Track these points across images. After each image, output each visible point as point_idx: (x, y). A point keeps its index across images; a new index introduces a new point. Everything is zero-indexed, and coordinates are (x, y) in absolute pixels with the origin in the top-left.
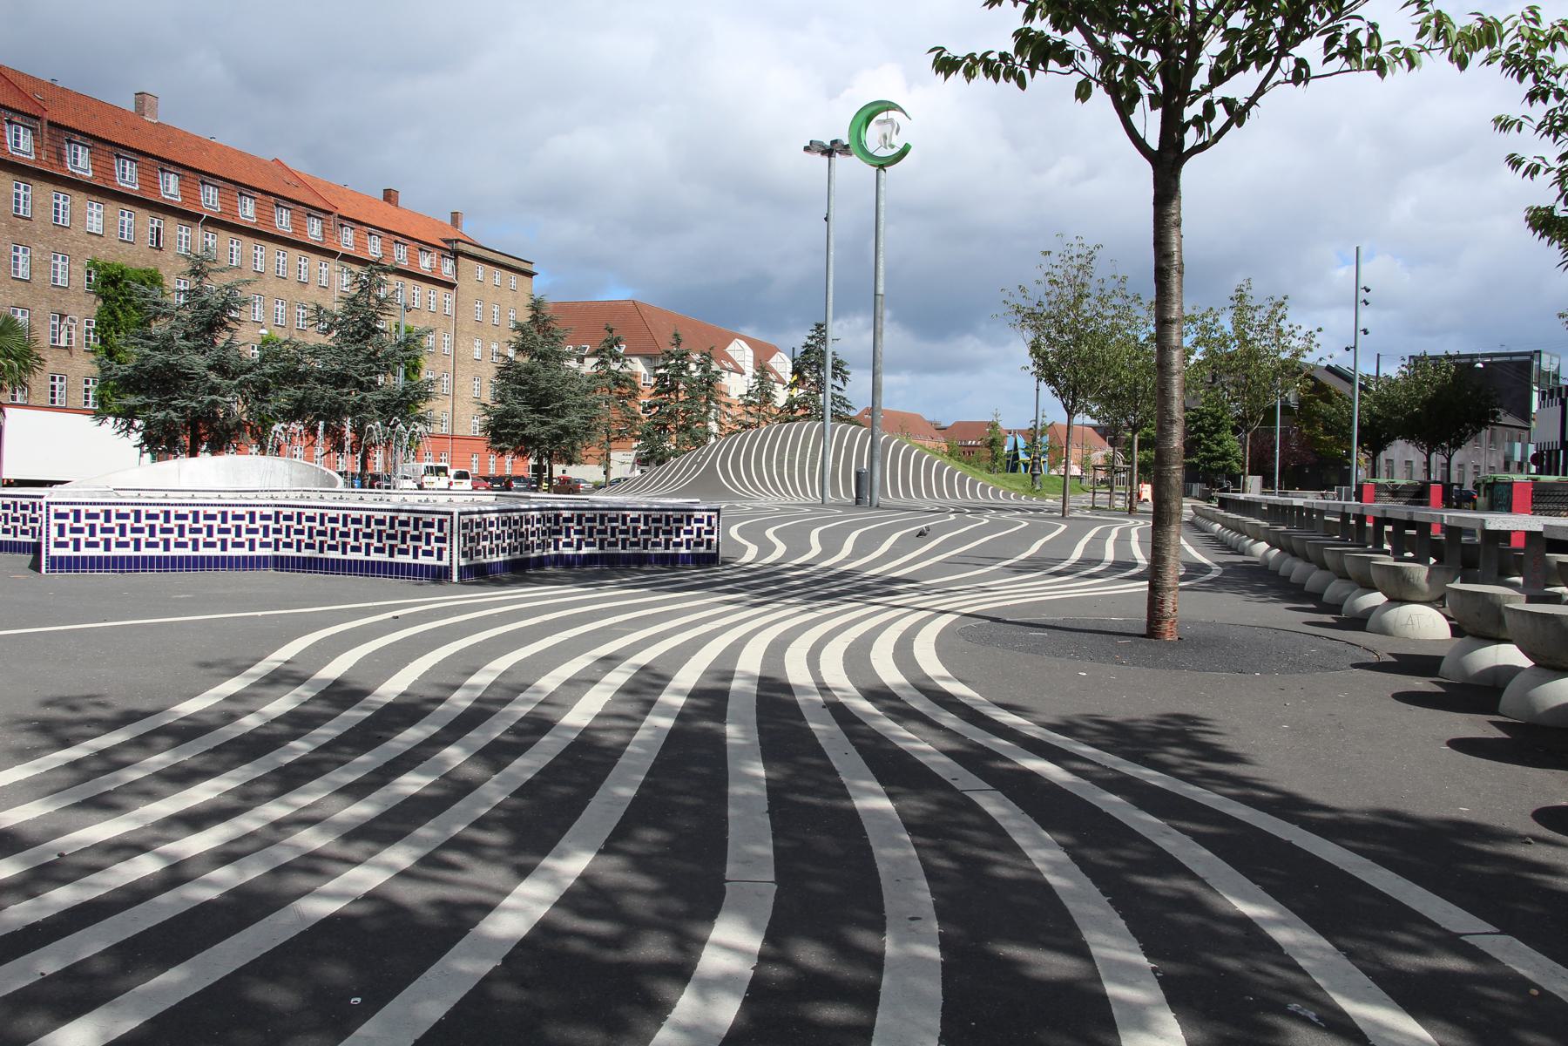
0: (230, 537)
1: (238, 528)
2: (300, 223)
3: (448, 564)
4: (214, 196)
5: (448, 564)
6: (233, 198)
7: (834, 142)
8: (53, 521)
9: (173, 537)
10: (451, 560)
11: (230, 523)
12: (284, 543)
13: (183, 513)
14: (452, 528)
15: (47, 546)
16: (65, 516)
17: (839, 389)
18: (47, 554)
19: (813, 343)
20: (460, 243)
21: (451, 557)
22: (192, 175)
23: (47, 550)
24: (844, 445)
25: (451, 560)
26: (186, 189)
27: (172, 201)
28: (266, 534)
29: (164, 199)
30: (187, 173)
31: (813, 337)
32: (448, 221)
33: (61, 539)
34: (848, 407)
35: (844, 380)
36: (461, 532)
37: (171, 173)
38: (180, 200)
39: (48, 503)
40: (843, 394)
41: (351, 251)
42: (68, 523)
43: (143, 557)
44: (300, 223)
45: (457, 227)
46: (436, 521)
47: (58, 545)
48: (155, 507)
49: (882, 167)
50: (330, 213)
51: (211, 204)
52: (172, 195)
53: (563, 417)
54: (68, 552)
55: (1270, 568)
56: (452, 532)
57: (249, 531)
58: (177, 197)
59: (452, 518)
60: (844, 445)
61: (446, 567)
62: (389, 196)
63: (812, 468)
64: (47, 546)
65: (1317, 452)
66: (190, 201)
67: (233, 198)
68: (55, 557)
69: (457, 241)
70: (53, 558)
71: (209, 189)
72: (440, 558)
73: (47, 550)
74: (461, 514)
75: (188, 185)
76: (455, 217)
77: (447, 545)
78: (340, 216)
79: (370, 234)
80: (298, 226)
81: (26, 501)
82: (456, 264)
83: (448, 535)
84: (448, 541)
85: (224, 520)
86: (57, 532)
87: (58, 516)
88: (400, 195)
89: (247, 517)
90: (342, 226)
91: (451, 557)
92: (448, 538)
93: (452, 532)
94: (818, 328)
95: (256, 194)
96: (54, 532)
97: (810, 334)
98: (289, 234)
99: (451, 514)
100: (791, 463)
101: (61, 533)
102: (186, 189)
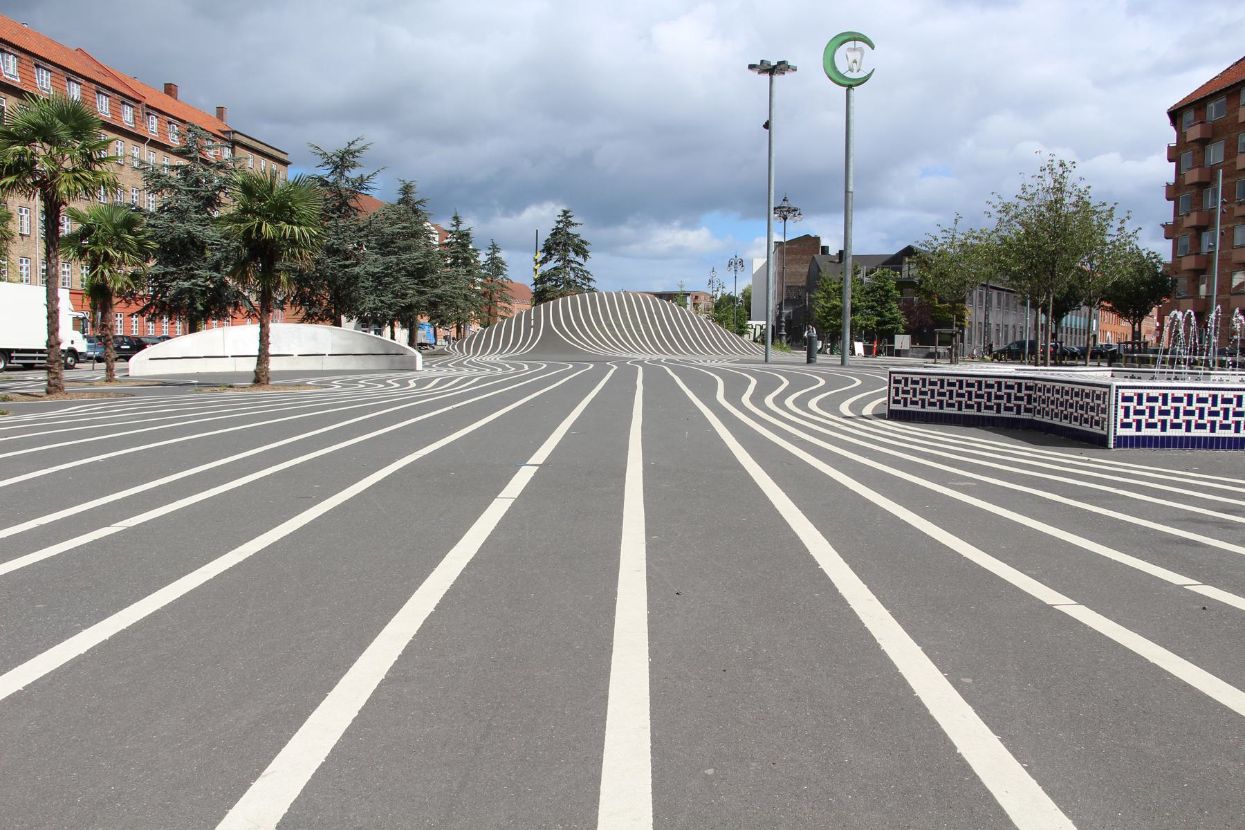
1: (1226, 411)
2: (117, 110)
4: (47, 80)
6: (63, 83)
7: (780, 63)
8: (1120, 404)
15: (1115, 427)
17: (580, 265)
18: (1115, 434)
19: (561, 225)
20: (236, 134)
22: (27, 57)
23: (1115, 430)
24: (654, 311)
26: (23, 71)
27: (13, 81)
29: (5, 78)
30: (23, 56)
31: (561, 221)
32: (214, 114)
33: (1126, 420)
34: (589, 279)
35: (585, 257)
37: (11, 54)
38: (19, 81)
39: (1117, 387)
40: (584, 268)
41: (156, 137)
43: (1192, 437)
44: (117, 110)
45: (222, 120)
47: (1125, 425)
48: (1130, 390)
49: (850, 87)
50: (138, 102)
51: (45, 87)
52: (12, 76)
54: (1131, 432)
58: (15, 77)
60: (654, 311)
62: (170, 89)
63: (638, 331)
64: (1115, 427)
65: (933, 317)
66: (29, 83)
67: (63, 83)
68: (1121, 436)
69: (234, 132)
70: (892, 410)
71: (42, 73)
73: (1115, 430)
75: (25, 67)
76: (220, 112)
77: (1106, 416)
78: (148, 106)
79: (170, 123)
80: (116, 112)
81: (916, 378)
82: (233, 152)
84: (1107, 413)
86: (1123, 414)
87: (1125, 399)
89: (1185, 399)
90: (148, 114)
94: (565, 214)
95: (80, 80)
96: (1121, 413)
97: (559, 219)
98: (108, 119)
99: (1109, 387)
100: (619, 326)
101: (1127, 415)
102: (23, 71)
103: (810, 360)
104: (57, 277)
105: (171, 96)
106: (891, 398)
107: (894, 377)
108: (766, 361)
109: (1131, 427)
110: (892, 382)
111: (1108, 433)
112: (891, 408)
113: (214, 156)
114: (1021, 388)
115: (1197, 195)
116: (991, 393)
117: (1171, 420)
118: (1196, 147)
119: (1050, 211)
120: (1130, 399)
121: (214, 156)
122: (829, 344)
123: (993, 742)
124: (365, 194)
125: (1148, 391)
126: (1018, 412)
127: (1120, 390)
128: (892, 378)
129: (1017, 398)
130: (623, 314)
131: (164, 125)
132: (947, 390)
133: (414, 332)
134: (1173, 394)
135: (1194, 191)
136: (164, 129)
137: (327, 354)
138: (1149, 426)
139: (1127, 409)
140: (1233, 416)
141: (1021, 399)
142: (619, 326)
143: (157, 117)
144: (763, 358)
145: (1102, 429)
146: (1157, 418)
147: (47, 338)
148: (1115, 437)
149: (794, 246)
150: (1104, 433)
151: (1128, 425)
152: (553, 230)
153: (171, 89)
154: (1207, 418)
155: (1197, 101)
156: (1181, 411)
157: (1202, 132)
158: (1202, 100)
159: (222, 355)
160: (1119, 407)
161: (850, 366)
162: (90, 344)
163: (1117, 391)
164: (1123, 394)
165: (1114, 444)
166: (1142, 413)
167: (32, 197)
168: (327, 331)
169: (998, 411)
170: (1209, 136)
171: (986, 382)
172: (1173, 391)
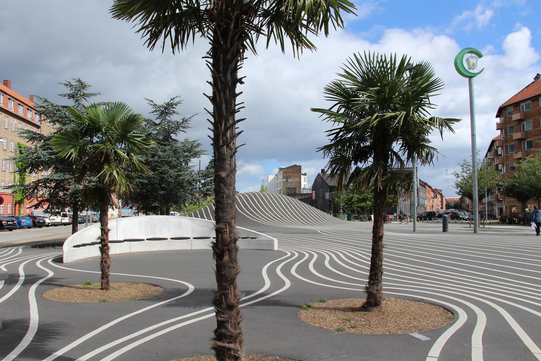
63: (286, 212)
100: (275, 210)
103: (445, 229)
104: (413, 173)
105: (7, 87)
108: (414, 231)
113: (31, 118)
115: (518, 144)
118: (516, 123)
121: (31, 118)
122: (347, 216)
123: (82, 341)
124: (182, 131)
130: (275, 204)
131: (6, 100)
133: (381, 225)
135: (516, 142)
136: (6, 102)
137: (169, 237)
142: (275, 210)
143: (3, 95)
144: (412, 229)
149: (289, 170)
152: (211, 160)
153: (7, 83)
155: (516, 103)
157: (521, 116)
158: (519, 102)
159: (115, 239)
161: (451, 233)
167: (117, 104)
168: (189, 221)
170: (523, 118)
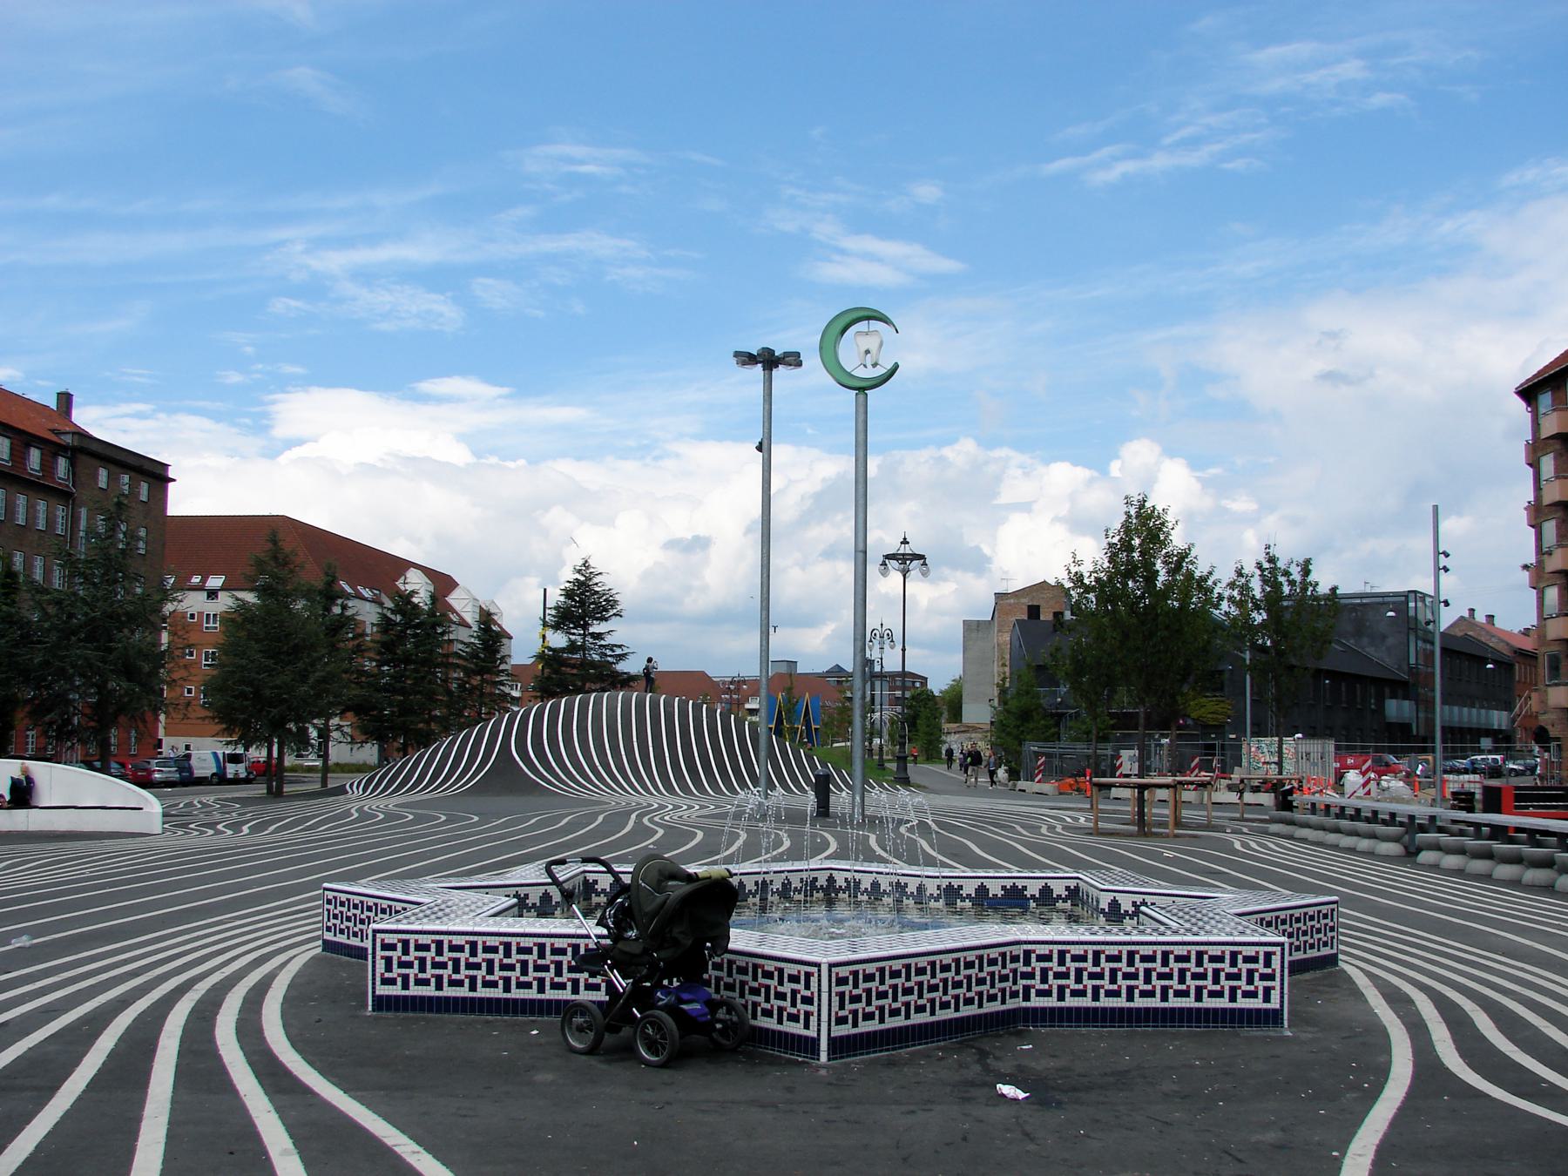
0: (480, 974)
1: (456, 962)
3: (1278, 1006)
5: (1278, 1006)
9: (480, 974)
10: (819, 1030)
11: (447, 955)
12: (1141, 991)
13: (493, 944)
14: (819, 985)
16: (392, 947)
21: (819, 1025)
23: (374, 988)
25: (819, 1030)
28: (1027, 989)
36: (835, 989)
42: (395, 955)
43: (479, 998)
46: (802, 973)
47: (385, 982)
53: (229, 672)
54: (396, 990)
55: (713, 878)
56: (819, 990)
57: (503, 967)
59: (819, 971)
61: (813, 1038)
70: (381, 997)
72: (1267, 999)
74: (831, 966)
77: (814, 1009)
83: (816, 995)
84: (816, 1004)
85: (474, 953)
87: (386, 947)
88: (74, 397)
91: (819, 1025)
92: (816, 999)
93: (819, 990)
96: (381, 965)
99: (818, 965)
101: (389, 968)
106: (833, 1014)
107: (837, 974)
109: (463, 986)
110: (834, 984)
111: (819, 1035)
112: (377, 993)
114: (442, 947)
116: (527, 961)
117: (416, 975)
119: (1162, 638)
120: (392, 947)
125: (416, 936)
126: (405, 986)
127: (378, 935)
128: (834, 975)
129: (402, 965)
132: (518, 961)
134: (518, 944)
138: (453, 983)
139: (388, 961)
140: (500, 970)
141: (511, 968)
145: (807, 1026)
146: (430, 972)
147: (1310, 839)
148: (373, 996)
150: (812, 1033)
151: (392, 982)
154: (464, 972)
156: (463, 963)
160: (378, 957)
162: (1446, 755)
163: (830, 971)
164: (383, 940)
165: (373, 1005)
166: (409, 965)
169: (405, 986)
171: (552, 945)
172: (450, 937)
